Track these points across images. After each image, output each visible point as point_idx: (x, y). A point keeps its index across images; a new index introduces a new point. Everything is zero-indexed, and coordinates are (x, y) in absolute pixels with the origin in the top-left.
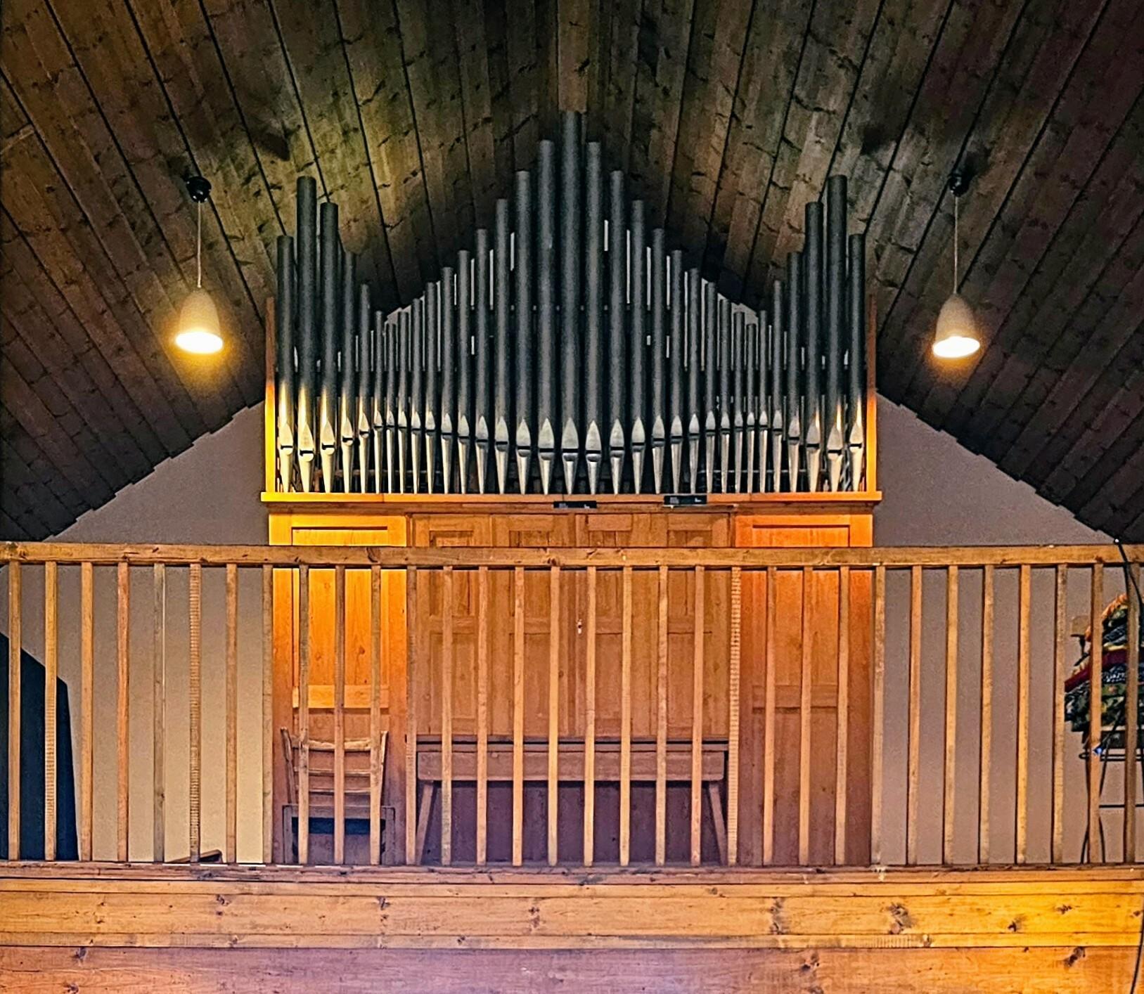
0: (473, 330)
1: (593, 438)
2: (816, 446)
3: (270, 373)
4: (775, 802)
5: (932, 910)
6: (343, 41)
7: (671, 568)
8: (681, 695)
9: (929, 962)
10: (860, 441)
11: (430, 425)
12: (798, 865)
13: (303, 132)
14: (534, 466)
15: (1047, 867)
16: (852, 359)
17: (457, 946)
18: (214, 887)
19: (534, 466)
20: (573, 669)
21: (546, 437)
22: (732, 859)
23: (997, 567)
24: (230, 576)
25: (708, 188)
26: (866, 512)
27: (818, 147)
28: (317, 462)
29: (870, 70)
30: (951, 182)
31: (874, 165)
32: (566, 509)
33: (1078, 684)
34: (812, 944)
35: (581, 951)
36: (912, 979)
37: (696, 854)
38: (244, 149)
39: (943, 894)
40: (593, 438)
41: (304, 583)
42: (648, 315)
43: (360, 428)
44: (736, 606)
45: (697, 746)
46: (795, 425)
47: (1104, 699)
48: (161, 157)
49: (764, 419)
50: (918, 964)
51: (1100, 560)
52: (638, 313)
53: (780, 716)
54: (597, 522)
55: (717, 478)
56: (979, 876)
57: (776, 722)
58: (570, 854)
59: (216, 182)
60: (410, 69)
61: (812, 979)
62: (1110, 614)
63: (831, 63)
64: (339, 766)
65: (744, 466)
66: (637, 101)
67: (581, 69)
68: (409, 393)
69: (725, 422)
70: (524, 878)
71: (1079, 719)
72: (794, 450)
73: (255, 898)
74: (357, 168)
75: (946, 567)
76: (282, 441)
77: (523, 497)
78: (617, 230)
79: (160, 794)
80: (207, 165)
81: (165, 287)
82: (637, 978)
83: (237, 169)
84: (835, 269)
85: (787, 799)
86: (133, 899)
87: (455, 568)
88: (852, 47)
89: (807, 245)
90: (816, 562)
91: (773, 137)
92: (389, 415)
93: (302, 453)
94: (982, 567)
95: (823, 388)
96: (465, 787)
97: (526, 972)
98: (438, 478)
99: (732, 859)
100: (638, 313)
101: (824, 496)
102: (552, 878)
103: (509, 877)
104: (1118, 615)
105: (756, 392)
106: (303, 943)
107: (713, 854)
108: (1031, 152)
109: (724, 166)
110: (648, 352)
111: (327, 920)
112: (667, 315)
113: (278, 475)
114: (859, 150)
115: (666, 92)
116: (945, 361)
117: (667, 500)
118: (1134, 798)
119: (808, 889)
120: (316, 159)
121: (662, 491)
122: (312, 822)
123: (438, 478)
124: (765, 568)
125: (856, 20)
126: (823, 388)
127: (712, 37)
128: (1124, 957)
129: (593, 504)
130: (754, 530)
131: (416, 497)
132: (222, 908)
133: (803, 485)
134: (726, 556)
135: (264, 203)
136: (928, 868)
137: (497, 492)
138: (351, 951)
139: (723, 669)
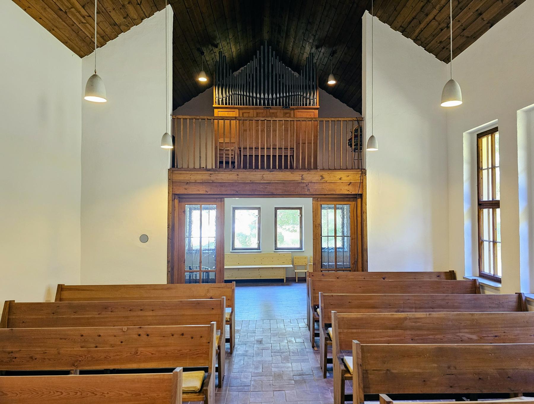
0: (249, 78)
1: (270, 96)
2: (308, 98)
3: (214, 84)
4: (302, 159)
5: (327, 176)
6: (228, 29)
7: (284, 121)
8: (286, 141)
9: (327, 185)
10: (316, 97)
11: (242, 94)
12: (305, 169)
13: (220, 44)
14: (260, 102)
15: (345, 169)
16: (314, 83)
17: (250, 182)
18: (209, 172)
19: (260, 102)
20: (268, 136)
21: (262, 96)
22: (295, 168)
23: (337, 121)
24: (212, 121)
25: (290, 53)
26: (317, 110)
27: (308, 48)
28: (222, 100)
29: (317, 37)
30: (331, 55)
31: (318, 51)
32: (266, 109)
33: (350, 140)
34: (308, 182)
35: (270, 183)
36: (324, 187)
37: (289, 167)
38: (210, 47)
39: (329, 174)
40: (270, 96)
41: (224, 122)
42: (280, 76)
43: (230, 94)
44: (295, 127)
45: (289, 149)
46: (305, 95)
47: (354, 142)
48: (196, 48)
49: (299, 93)
50: (325, 185)
51: (353, 120)
52: (278, 75)
53: (302, 144)
54: (271, 111)
55: (291, 103)
56: (334, 171)
57: (302, 145)
58: (268, 167)
59: (205, 52)
60: (239, 33)
61: (308, 188)
62: (356, 128)
63: (310, 35)
64: (230, 153)
65: (296, 101)
66: (277, 38)
67: (268, 32)
68: (238, 88)
69: (293, 94)
70: (261, 171)
71: (351, 145)
72: (305, 99)
73: (216, 174)
74: (229, 49)
75: (329, 121)
76: (216, 96)
77: (258, 106)
78: (274, 59)
79: (200, 157)
80: (204, 49)
81: (196, 69)
82: (279, 187)
83: (209, 50)
84: (311, 68)
85: (304, 159)
86: (196, 174)
87: (249, 120)
88: (314, 32)
89: (306, 64)
90: (308, 120)
91: (301, 45)
92: (235, 92)
93: (220, 98)
94: (335, 121)
95: (309, 88)
96: (251, 156)
97: (261, 186)
98: (244, 103)
99: (295, 168)
100: (278, 75)
101: (310, 107)
102: (265, 171)
103: (258, 171)
104: (357, 129)
105: (298, 89)
106: (224, 182)
107: (292, 167)
108: (344, 50)
109: (292, 49)
110: (280, 82)
111: (228, 178)
112: (283, 76)
113: (216, 102)
114: (315, 48)
115: (282, 37)
116: (330, 84)
117: (283, 107)
118: (359, 158)
119: (307, 173)
120: (222, 48)
121: (282, 106)
122: (226, 162)
123: (244, 103)
124: (300, 121)
125: (314, 29)
126: (309, 88)
127: (290, 29)
128: (358, 184)
129: (270, 108)
130: (298, 113)
131: (240, 106)
132: (211, 176)
133: (306, 105)
134: (294, 119)
135: (213, 55)
136: (326, 169)
137: (254, 105)
138: (232, 183)
139: (293, 136)
